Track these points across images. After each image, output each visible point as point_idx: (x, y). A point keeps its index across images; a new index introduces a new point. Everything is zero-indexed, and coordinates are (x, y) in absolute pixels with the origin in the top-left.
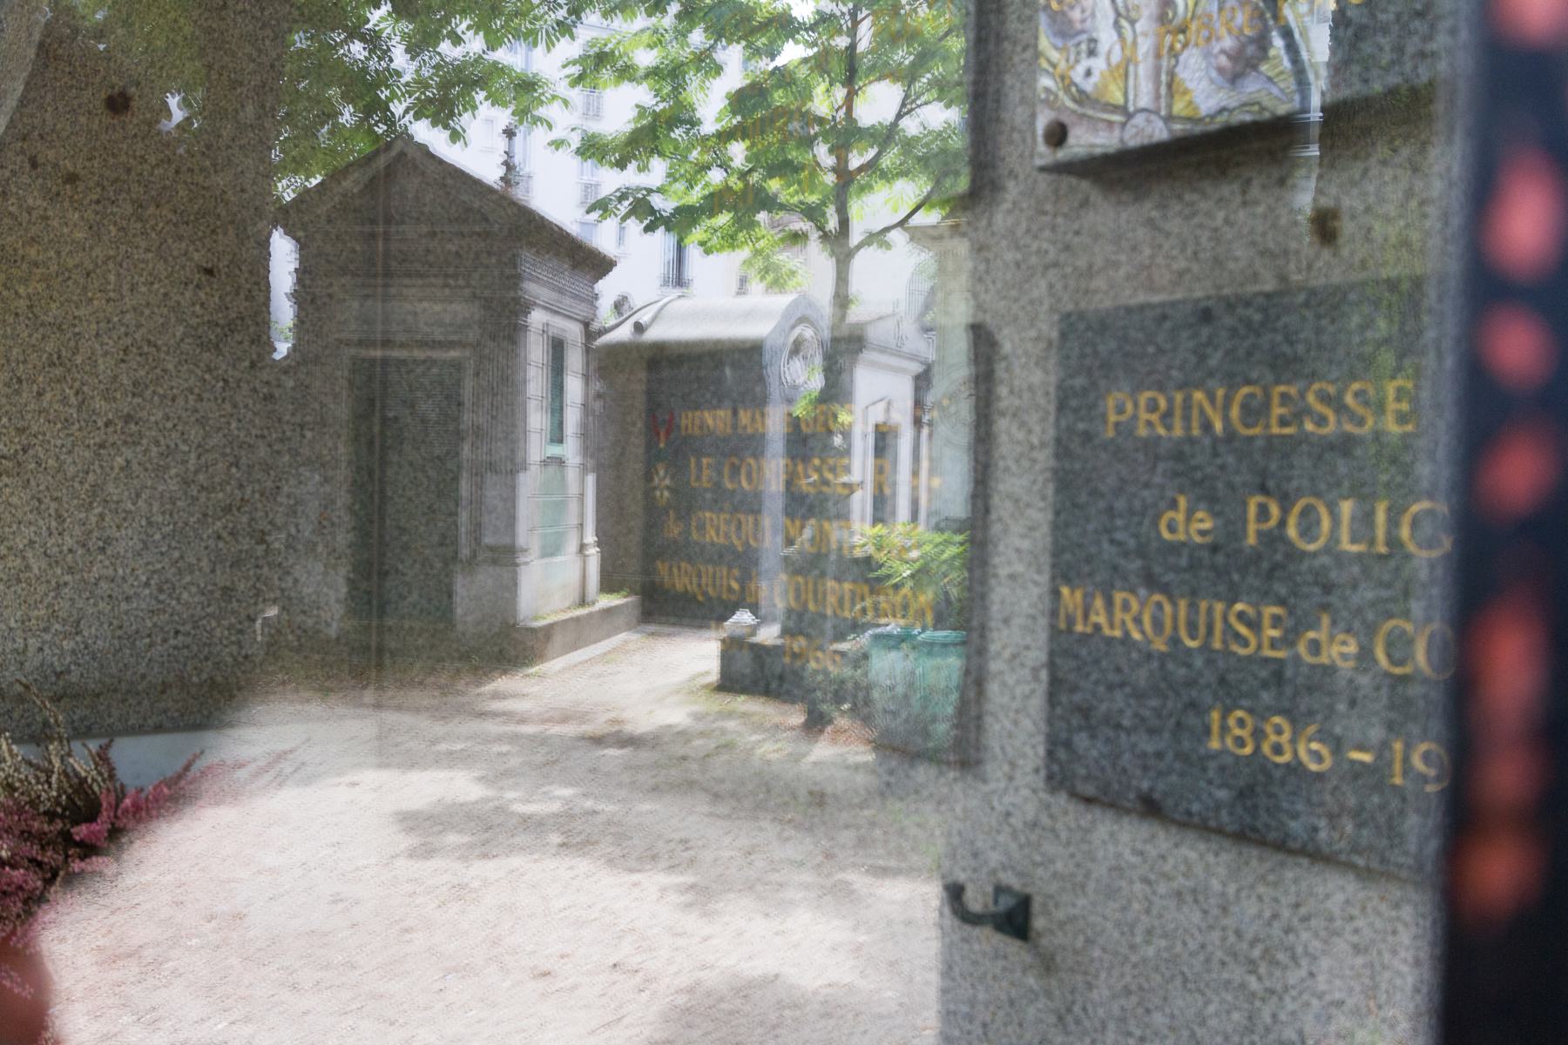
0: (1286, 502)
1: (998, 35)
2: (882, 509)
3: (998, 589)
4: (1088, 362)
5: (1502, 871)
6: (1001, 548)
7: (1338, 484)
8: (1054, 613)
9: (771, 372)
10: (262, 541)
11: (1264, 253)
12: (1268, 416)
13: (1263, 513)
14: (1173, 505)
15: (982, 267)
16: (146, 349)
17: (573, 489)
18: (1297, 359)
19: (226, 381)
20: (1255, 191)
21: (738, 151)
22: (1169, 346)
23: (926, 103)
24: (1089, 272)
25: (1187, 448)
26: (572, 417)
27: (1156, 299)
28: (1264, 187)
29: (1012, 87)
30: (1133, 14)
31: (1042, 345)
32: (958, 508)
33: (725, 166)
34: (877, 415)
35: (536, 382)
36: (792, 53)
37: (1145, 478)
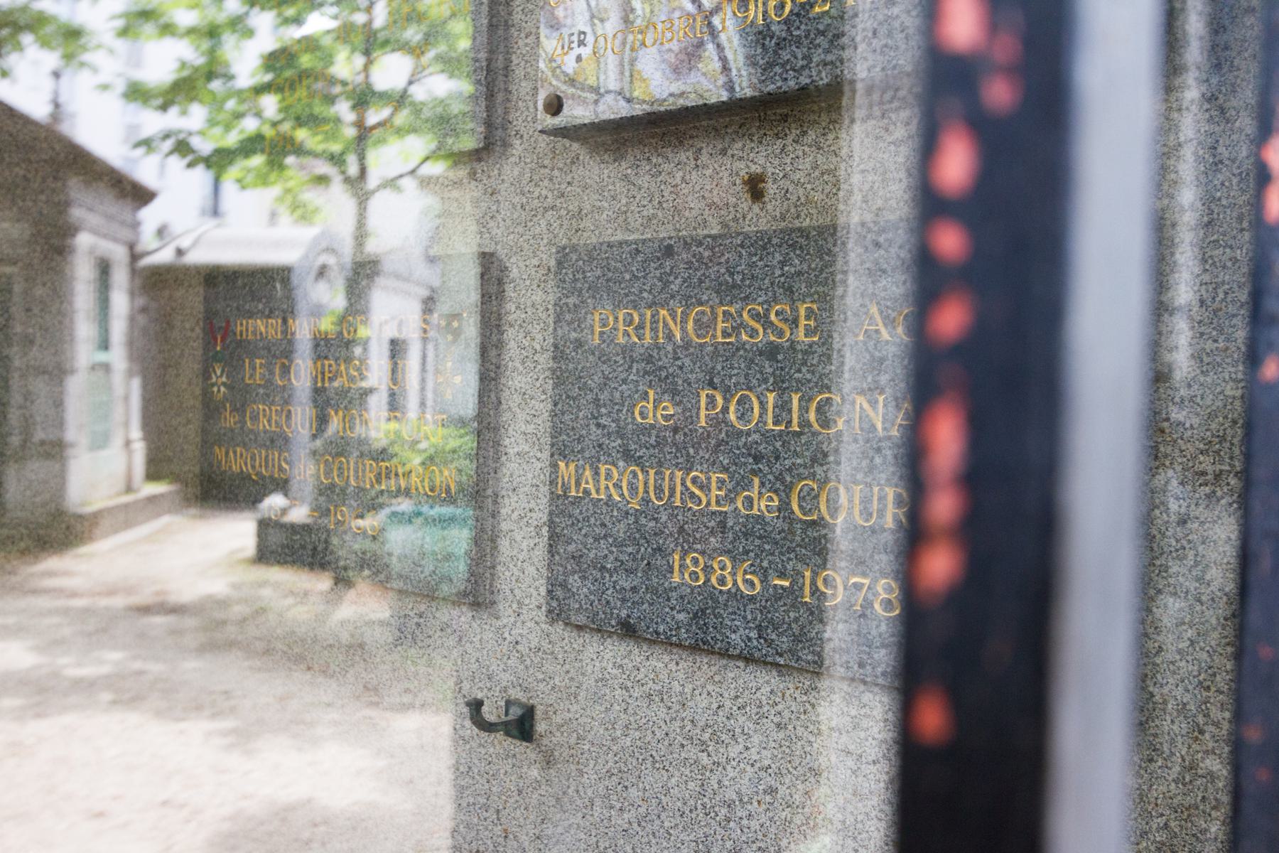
1: (506, 21)
2: (395, 404)
5: (940, 566)
7: (765, 381)
9: (298, 294)
12: (715, 329)
13: (711, 401)
18: (734, 286)
20: (704, 158)
21: (270, 104)
23: (431, 74)
24: (579, 215)
26: (118, 328)
30: (604, 16)
32: (468, 406)
33: (258, 114)
34: (391, 332)
37: (623, 376)
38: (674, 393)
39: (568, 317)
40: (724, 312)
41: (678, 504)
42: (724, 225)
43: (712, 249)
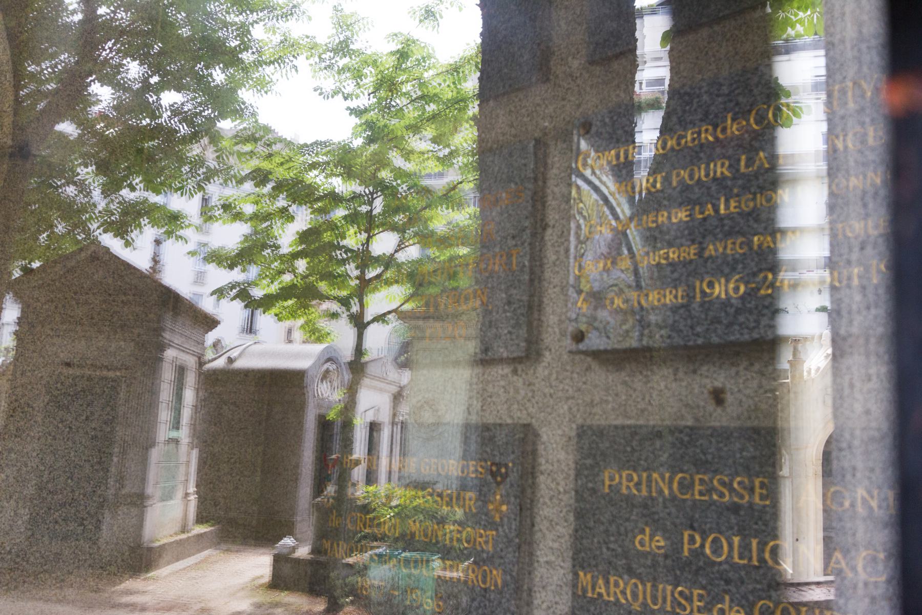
0: (704, 535)
3: (540, 569)
4: (593, 452)
6: (541, 546)
8: (575, 586)
10: (82, 524)
11: (687, 405)
12: (693, 490)
13: (692, 540)
14: (642, 531)
15: (530, 394)
16: (26, 409)
17: (183, 458)
18: (707, 462)
19: (70, 428)
20: (681, 374)
22: (638, 448)
24: (592, 404)
25: (649, 503)
26: (187, 414)
27: (629, 422)
28: (686, 373)
29: (548, 304)
31: (565, 439)
33: (293, 271)
34: (370, 417)
35: (166, 393)
36: (340, 213)
38: (665, 531)
39: (586, 472)
40: (700, 480)
41: (669, 609)
42: (697, 419)
43: (690, 436)
